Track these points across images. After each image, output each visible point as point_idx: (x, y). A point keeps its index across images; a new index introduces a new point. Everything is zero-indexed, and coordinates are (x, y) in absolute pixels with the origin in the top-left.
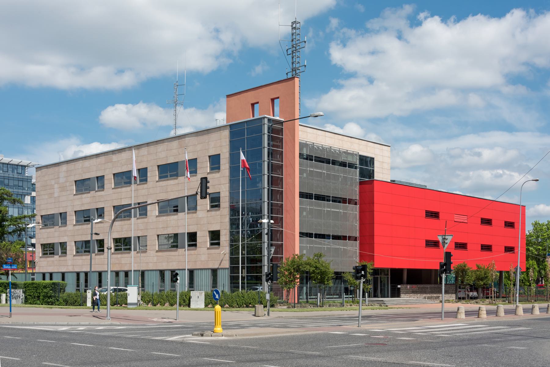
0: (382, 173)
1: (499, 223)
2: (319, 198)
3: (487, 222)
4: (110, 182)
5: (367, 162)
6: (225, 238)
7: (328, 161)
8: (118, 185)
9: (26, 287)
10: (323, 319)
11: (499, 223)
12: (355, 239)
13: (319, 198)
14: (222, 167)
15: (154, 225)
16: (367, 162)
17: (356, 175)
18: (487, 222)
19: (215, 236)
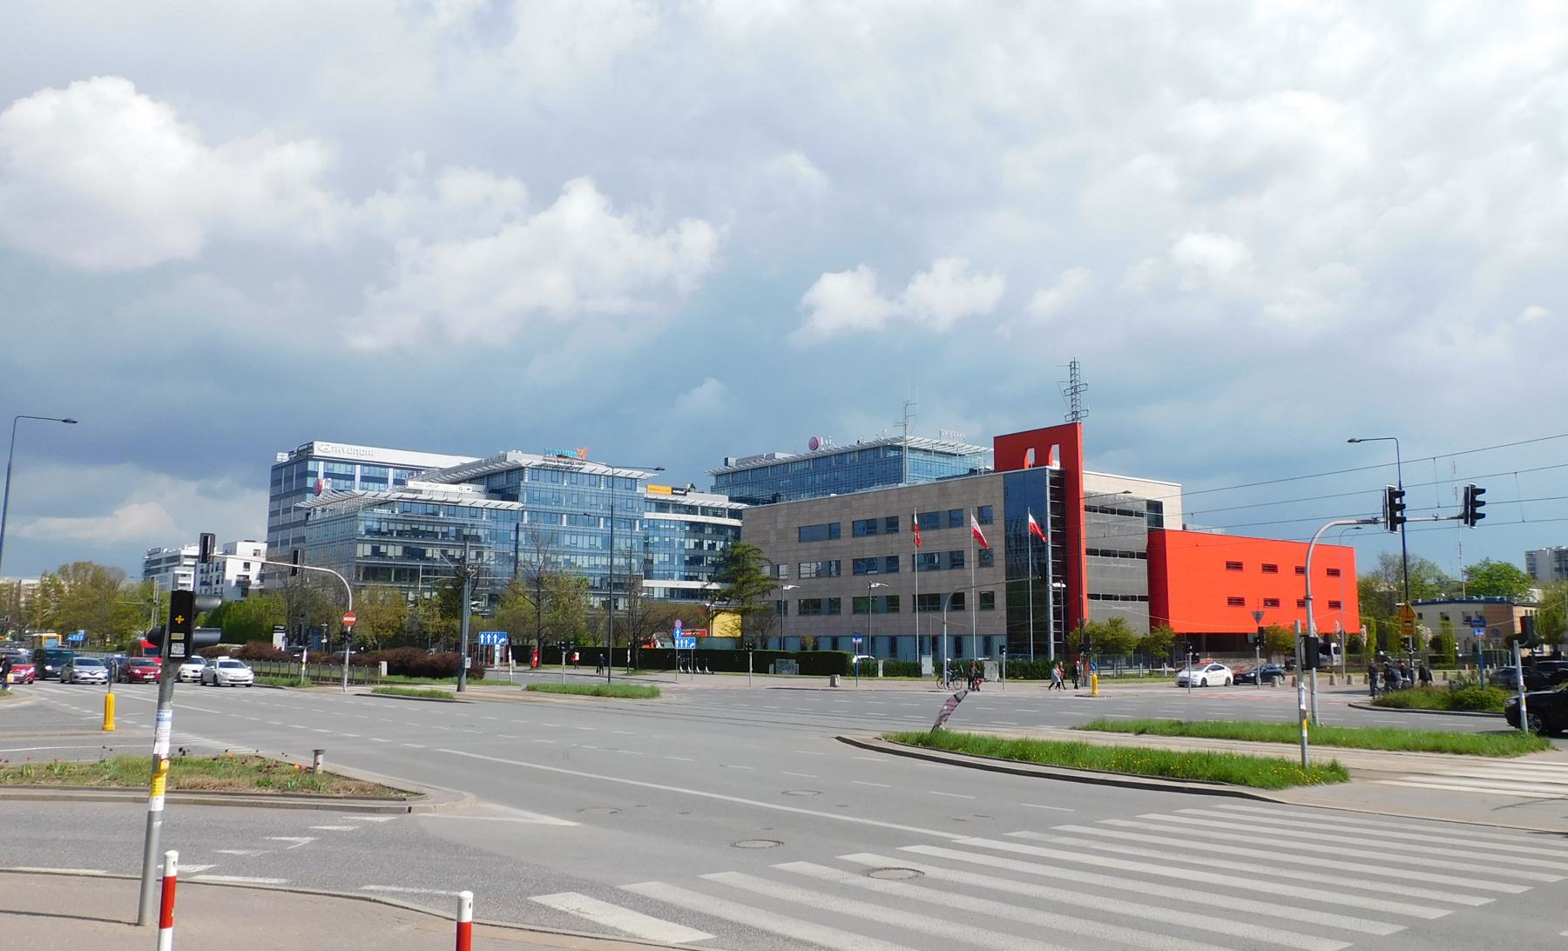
0: (1172, 522)
1: (1286, 570)
2: (1106, 553)
3: (1272, 568)
4: (847, 604)
5: (1156, 507)
6: (1000, 600)
7: (1113, 512)
8: (856, 611)
9: (797, 657)
10: (1163, 772)
11: (1286, 570)
12: (1088, 509)
13: (1106, 553)
14: (996, 563)
15: (904, 545)
16: (1156, 507)
17: (1143, 525)
18: (1272, 568)
19: (987, 600)
